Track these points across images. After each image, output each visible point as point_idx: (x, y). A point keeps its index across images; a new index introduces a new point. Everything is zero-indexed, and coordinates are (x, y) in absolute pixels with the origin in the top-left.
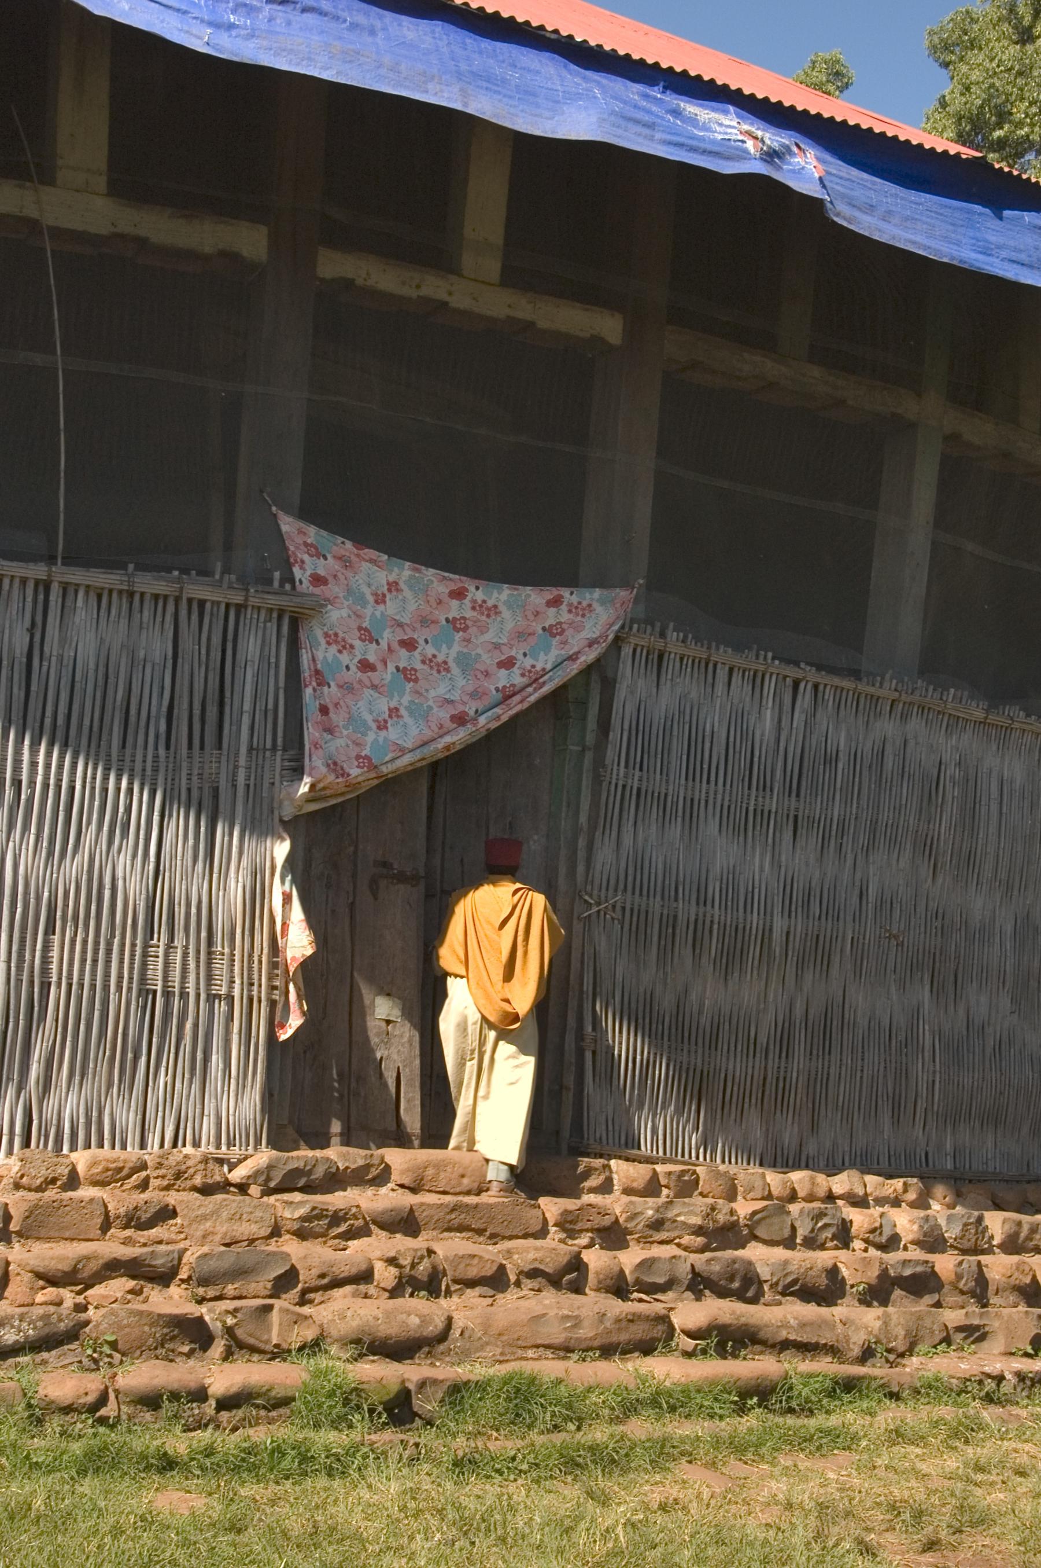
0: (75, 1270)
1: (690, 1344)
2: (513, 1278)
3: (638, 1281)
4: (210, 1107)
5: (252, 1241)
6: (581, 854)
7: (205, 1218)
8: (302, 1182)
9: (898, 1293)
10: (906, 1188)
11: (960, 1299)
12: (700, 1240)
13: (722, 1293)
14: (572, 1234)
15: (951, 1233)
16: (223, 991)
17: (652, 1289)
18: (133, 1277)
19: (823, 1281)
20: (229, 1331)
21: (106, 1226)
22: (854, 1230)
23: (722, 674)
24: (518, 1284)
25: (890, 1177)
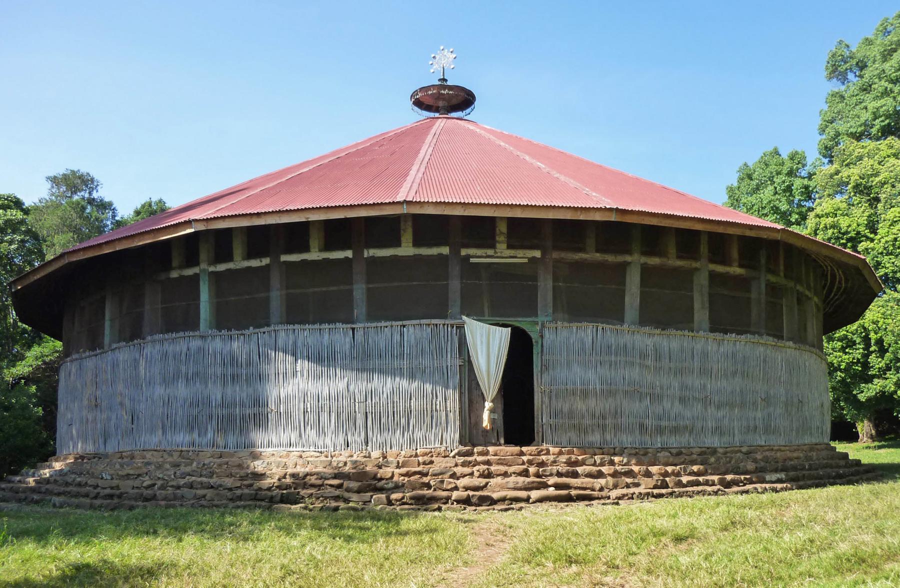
5: (451, 467)
12: (565, 465)
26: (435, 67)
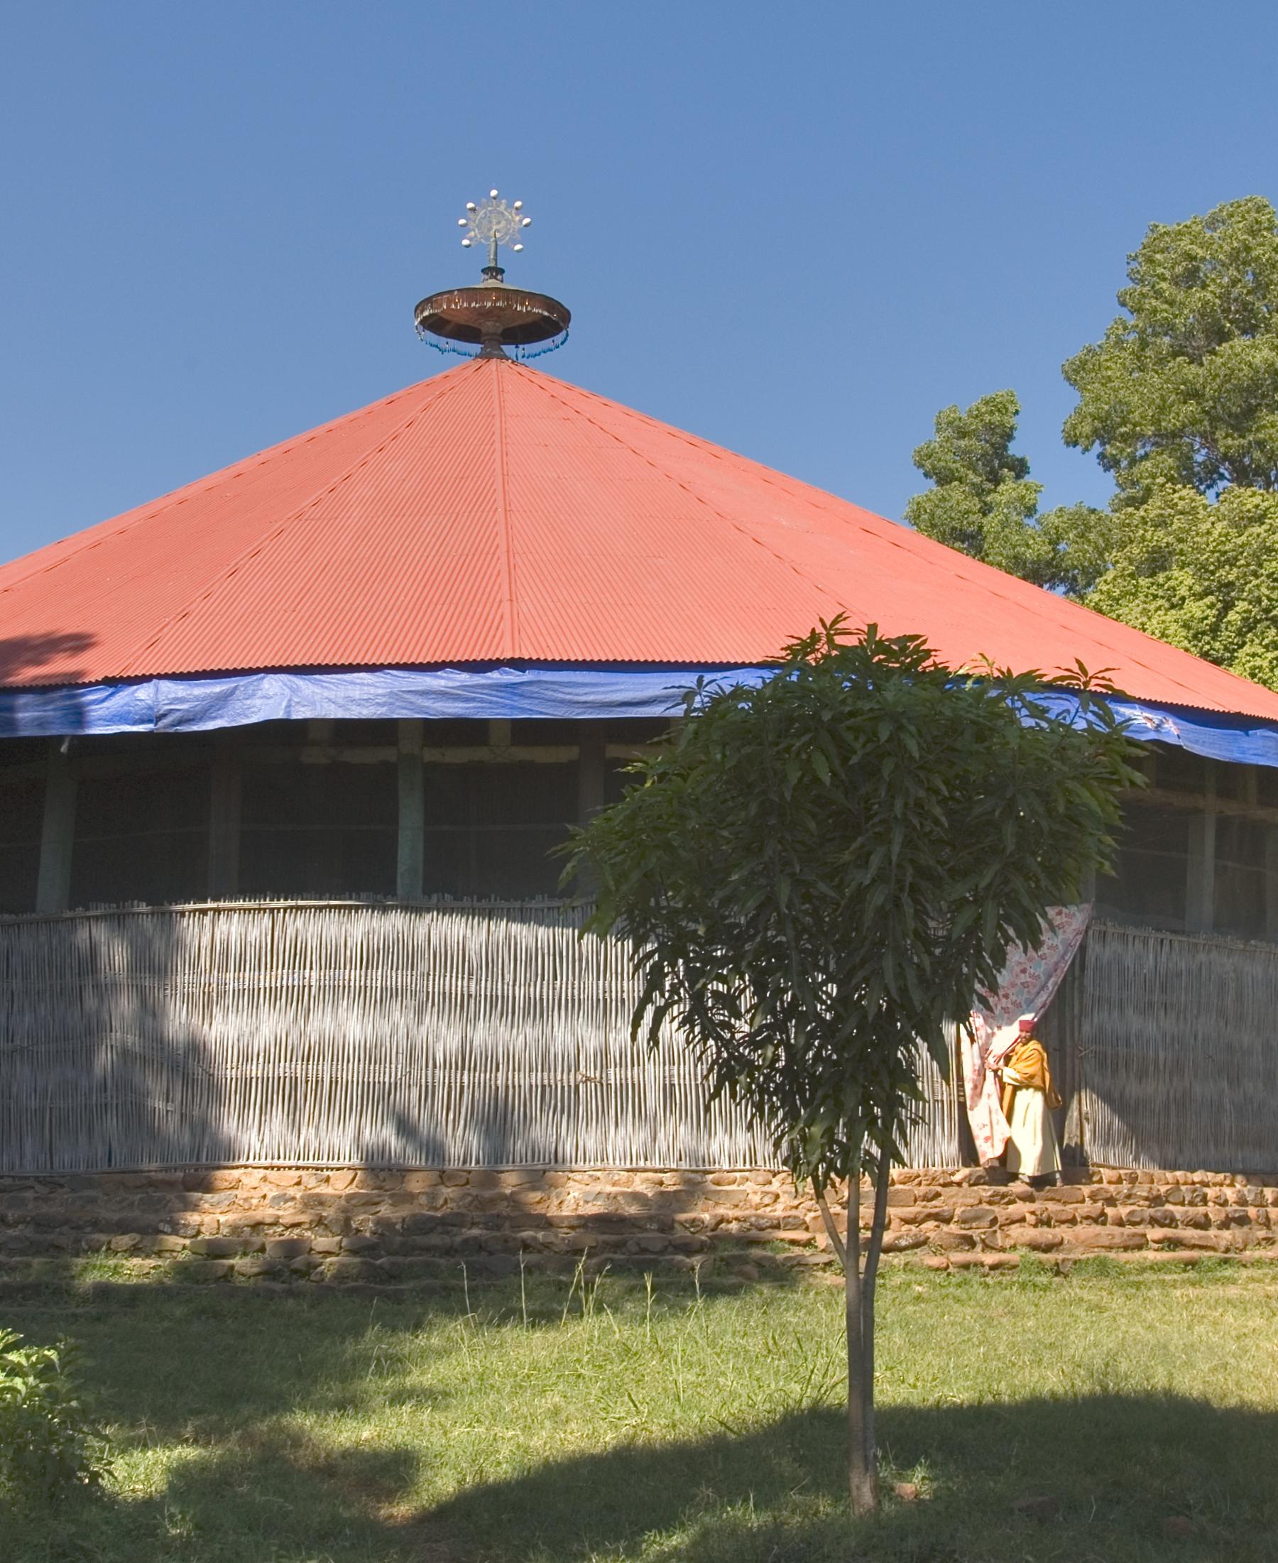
0: (916, 1218)
1: (1156, 1246)
2: (1079, 1220)
3: (1128, 1221)
4: (937, 1150)
6: (1076, 1028)
7: (952, 1196)
8: (982, 1181)
9: (1233, 1225)
10: (1225, 1177)
11: (1260, 1227)
12: (1147, 1203)
13: (1162, 1225)
14: (1095, 1201)
15: (1250, 1198)
16: (939, 1098)
17: (1134, 1224)
18: (936, 1220)
19: (1203, 1220)
20: (983, 1241)
21: (915, 1201)
22: (1208, 1198)
23: (1130, 939)
24: (1081, 1222)
25: (1217, 1172)
26: (472, 234)
